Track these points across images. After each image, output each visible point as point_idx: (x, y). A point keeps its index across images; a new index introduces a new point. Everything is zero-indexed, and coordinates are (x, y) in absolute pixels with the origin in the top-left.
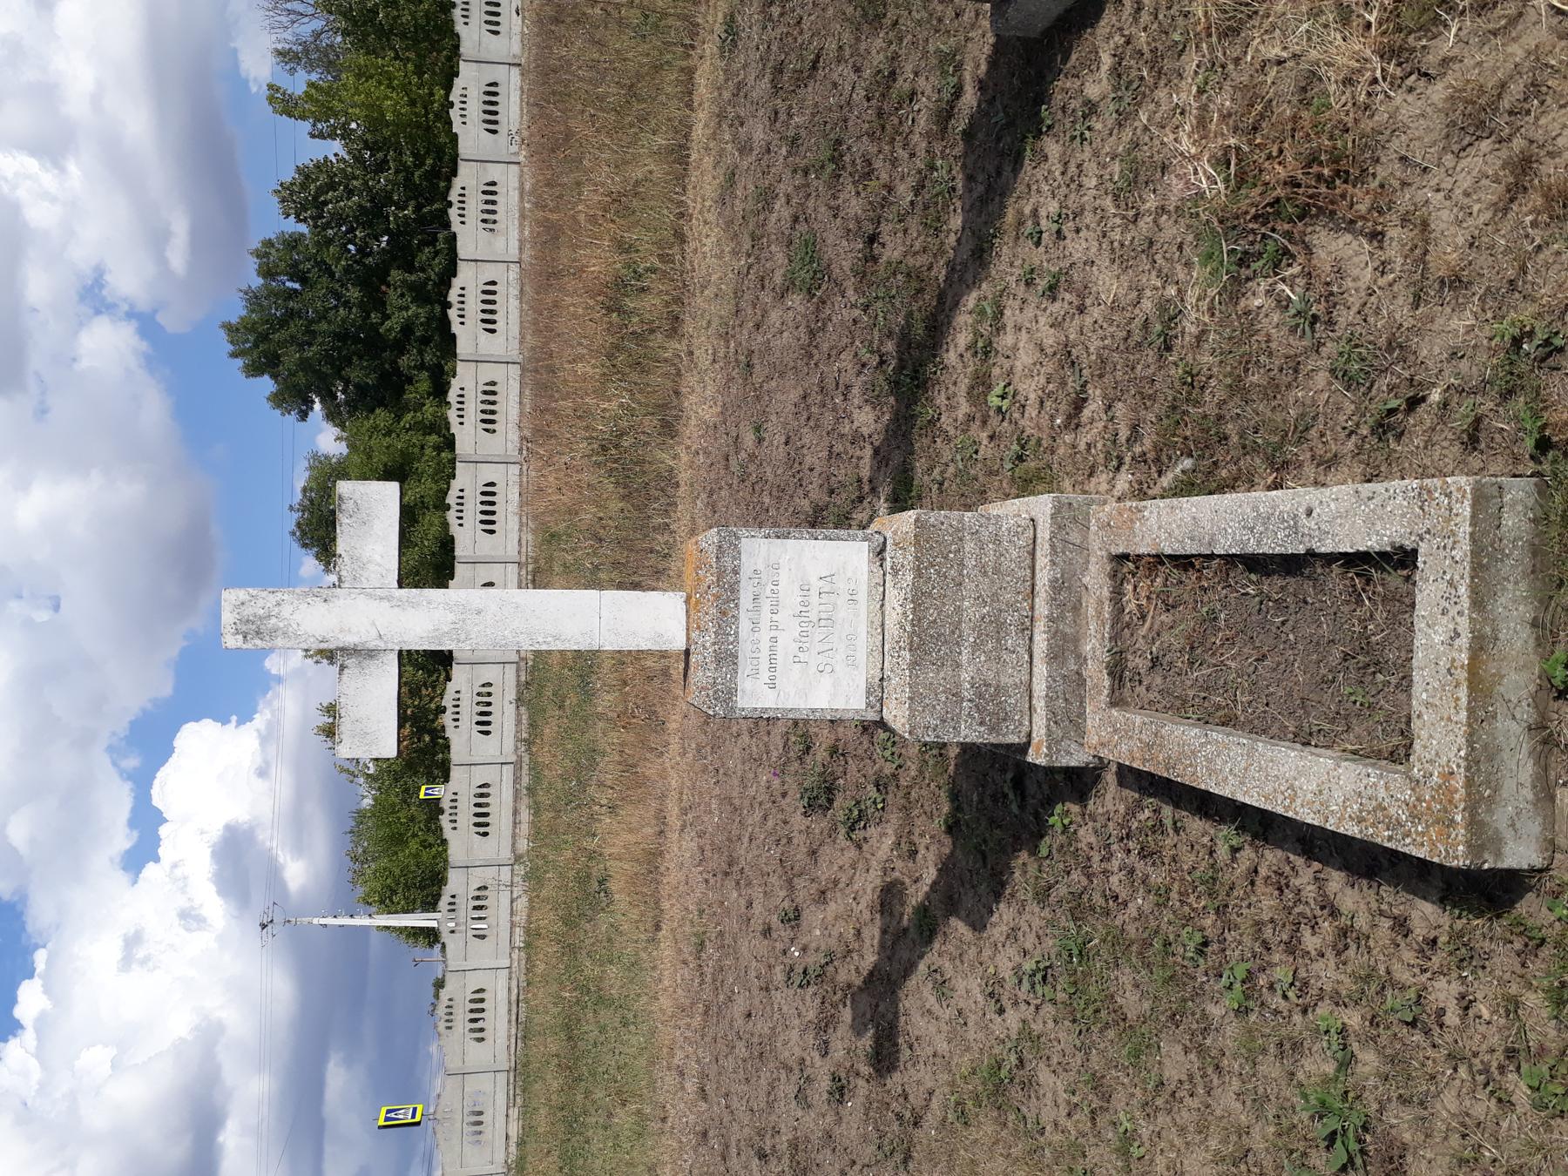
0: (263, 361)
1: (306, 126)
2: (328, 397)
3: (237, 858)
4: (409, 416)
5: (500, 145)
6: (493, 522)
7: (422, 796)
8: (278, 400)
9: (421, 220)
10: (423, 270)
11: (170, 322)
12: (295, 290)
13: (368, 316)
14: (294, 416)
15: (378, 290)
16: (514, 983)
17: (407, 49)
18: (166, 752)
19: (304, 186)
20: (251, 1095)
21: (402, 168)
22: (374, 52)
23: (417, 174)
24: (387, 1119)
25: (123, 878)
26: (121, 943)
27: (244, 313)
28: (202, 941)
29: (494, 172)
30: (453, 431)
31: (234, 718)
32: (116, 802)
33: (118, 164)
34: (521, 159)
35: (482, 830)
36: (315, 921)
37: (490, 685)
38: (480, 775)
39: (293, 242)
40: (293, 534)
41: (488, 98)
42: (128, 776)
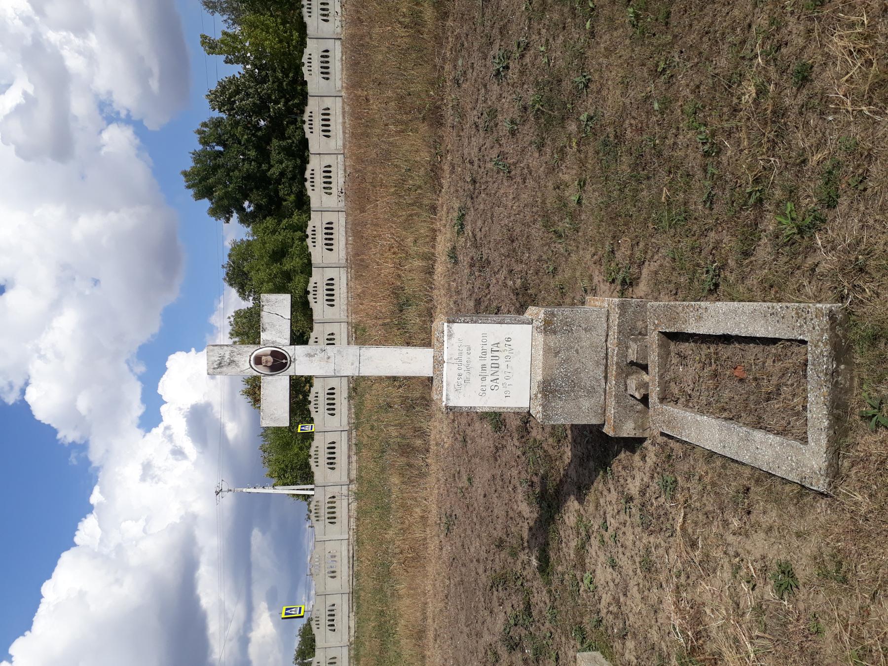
0: (204, 192)
1: (223, 57)
2: (241, 210)
3: (199, 419)
4: (285, 221)
5: (333, 201)
6: (333, 300)
7: (299, 431)
8: (214, 212)
9: (289, 111)
10: (289, 138)
11: (153, 124)
12: (220, 152)
13: (261, 165)
14: (223, 220)
15: (265, 149)
16: (351, 547)
17: (277, 10)
18: (162, 370)
19: (223, 93)
20: (211, 545)
21: (276, 80)
22: (259, 11)
23: (285, 83)
24: (286, 614)
25: (139, 432)
26: (140, 467)
27: (193, 164)
28: (184, 466)
29: (328, 102)
30: (307, 136)
31: (193, 350)
32: (134, 392)
33: (116, 35)
34: (343, 94)
35: (325, 18)
36: (244, 490)
37: (328, 109)
38: (330, 438)
39: (218, 123)
40: (225, 279)
41: (323, 59)
42: (141, 378)
